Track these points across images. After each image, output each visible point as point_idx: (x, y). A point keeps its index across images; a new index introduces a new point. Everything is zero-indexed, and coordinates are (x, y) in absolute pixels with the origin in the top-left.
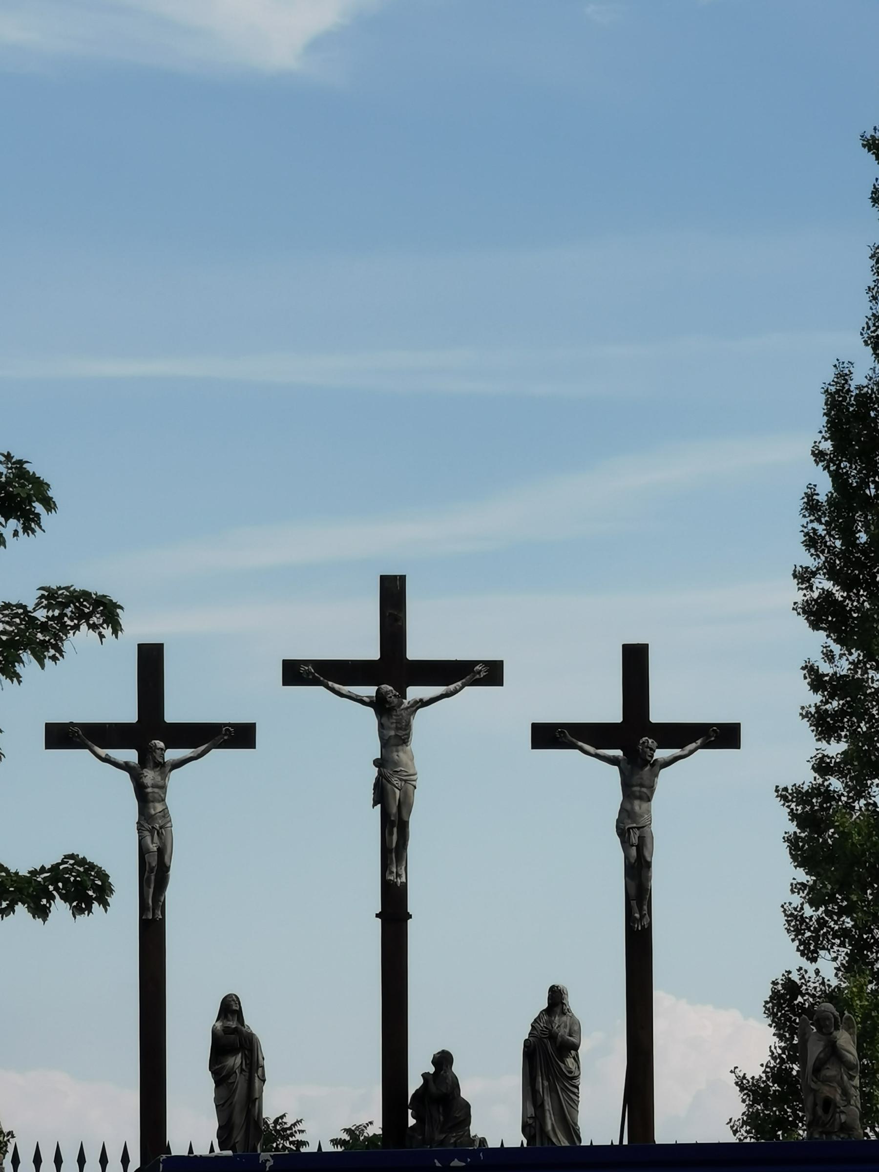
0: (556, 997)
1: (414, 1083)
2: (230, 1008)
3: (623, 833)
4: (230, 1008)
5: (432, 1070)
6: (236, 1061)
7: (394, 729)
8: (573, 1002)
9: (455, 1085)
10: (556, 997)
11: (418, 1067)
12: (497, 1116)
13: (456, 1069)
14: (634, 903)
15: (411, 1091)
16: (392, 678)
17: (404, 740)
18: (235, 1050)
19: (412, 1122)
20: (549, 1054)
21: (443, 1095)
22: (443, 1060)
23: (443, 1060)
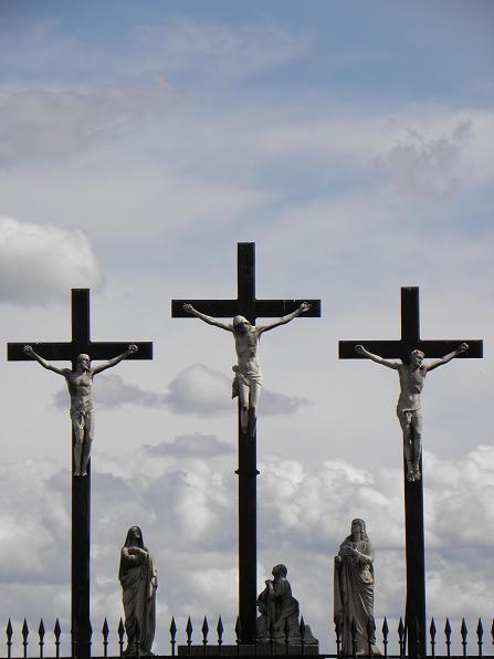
0: (357, 524)
1: (261, 588)
2: (134, 538)
3: (402, 416)
4: (134, 538)
5: (272, 578)
7: (246, 348)
8: (369, 530)
9: (288, 588)
12: (316, 607)
13: (289, 578)
14: (409, 463)
15: (259, 592)
16: (246, 310)
18: (136, 569)
19: (259, 614)
20: (351, 568)
23: (280, 571)
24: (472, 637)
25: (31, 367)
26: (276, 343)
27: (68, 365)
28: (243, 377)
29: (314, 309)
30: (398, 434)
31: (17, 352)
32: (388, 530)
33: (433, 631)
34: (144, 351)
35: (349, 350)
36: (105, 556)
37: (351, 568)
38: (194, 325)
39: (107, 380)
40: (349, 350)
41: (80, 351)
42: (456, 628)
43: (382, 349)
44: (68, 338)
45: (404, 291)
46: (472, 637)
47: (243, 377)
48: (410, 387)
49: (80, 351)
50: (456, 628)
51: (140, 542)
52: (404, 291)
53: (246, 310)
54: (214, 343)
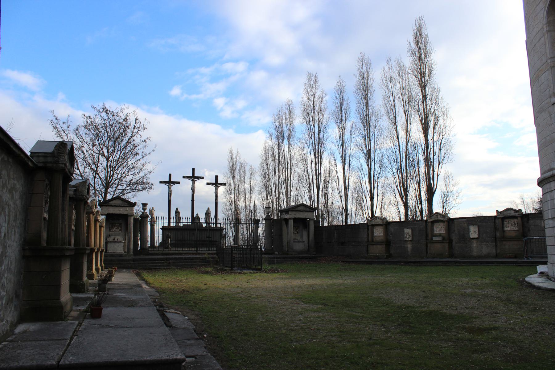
0: (208, 208)
1: (195, 216)
2: (177, 209)
4: (177, 209)
8: (210, 209)
10: (208, 208)
14: (37, 154)
16: (193, 178)
18: (177, 212)
20: (208, 214)
21: (198, 218)
22: (197, 214)
23: (197, 214)
26: (198, 183)
29: (203, 178)
31: (161, 182)
34: (179, 183)
35: (208, 184)
40: (208, 184)
41: (170, 183)
49: (170, 183)
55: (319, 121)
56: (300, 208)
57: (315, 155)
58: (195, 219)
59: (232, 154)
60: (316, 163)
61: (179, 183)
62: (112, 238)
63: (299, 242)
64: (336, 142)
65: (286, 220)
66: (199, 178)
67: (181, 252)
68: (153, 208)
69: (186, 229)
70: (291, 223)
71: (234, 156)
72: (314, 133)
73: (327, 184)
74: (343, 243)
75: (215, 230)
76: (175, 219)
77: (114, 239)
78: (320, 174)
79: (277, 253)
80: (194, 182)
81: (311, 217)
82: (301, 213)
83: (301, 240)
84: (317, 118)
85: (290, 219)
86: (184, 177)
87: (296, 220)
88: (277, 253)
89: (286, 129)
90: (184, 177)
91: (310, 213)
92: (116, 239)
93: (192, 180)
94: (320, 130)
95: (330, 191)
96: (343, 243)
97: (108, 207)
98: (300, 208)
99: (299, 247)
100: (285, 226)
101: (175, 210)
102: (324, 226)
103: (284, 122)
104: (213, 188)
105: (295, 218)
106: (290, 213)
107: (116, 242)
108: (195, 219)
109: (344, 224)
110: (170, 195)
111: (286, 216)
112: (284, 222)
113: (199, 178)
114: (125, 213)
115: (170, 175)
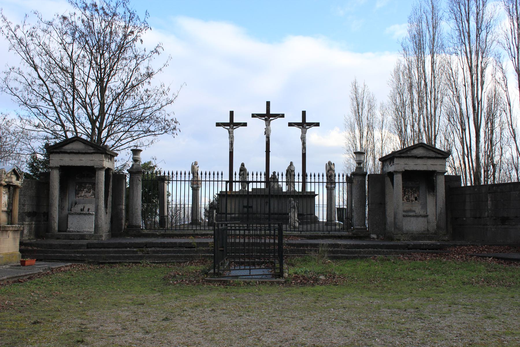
0: (291, 164)
1: (270, 176)
2: (243, 165)
3: (301, 138)
4: (243, 165)
6: (242, 172)
8: (294, 164)
10: (291, 164)
11: (271, 174)
12: (282, 180)
17: (269, 125)
18: (243, 169)
20: (290, 172)
21: (275, 178)
22: (274, 173)
23: (274, 173)
24: (255, 176)
25: (221, 128)
26: (275, 123)
27: (229, 127)
28: (267, 134)
29: (283, 116)
30: (301, 143)
31: (218, 125)
32: (298, 170)
33: (235, 174)
34: (245, 124)
35: (290, 124)
36: (236, 169)
37: (290, 172)
38: (257, 119)
39: (237, 131)
40: (290, 124)
41: (231, 125)
42: (175, 173)
43: (298, 124)
44: (229, 122)
45: (303, 112)
46: (255, 176)
47: (267, 134)
48: (304, 133)
49: (231, 125)
50: (175, 173)
51: (244, 166)
52: (303, 112)
53: (268, 116)
54: (261, 123)
55: (478, 14)
56: (415, 152)
57: (471, 71)
58: (271, 179)
59: (356, 92)
60: (472, 84)
61: (245, 124)
62: (80, 207)
63: (417, 216)
64: (504, 41)
65: (391, 175)
66: (276, 116)
67: (196, 232)
68: (196, 164)
69: (259, 196)
70: (398, 179)
71: (360, 91)
72: (469, 33)
73: (491, 118)
74: (504, 220)
75: (301, 196)
76: (325, 177)
77: (82, 210)
78: (480, 102)
79: (374, 236)
80: (268, 121)
81: (438, 168)
82: (419, 161)
83: (422, 213)
84: (474, 9)
85: (396, 172)
86: (253, 116)
87: (408, 175)
88: (374, 236)
89: (427, 38)
90: (253, 116)
91: (438, 162)
92: (86, 209)
93: (266, 120)
94: (479, 29)
95: (497, 130)
96: (504, 220)
97: (61, 155)
98: (415, 152)
99: (414, 225)
100: (390, 183)
101: (240, 166)
102: (466, 187)
103: (424, 25)
104: (298, 131)
105: (406, 171)
106: (396, 161)
107: (85, 214)
108: (271, 179)
109: (300, 190)
110: (231, 144)
111: (391, 169)
112: (388, 179)
113: (276, 116)
114: (89, 164)
115: (232, 113)
